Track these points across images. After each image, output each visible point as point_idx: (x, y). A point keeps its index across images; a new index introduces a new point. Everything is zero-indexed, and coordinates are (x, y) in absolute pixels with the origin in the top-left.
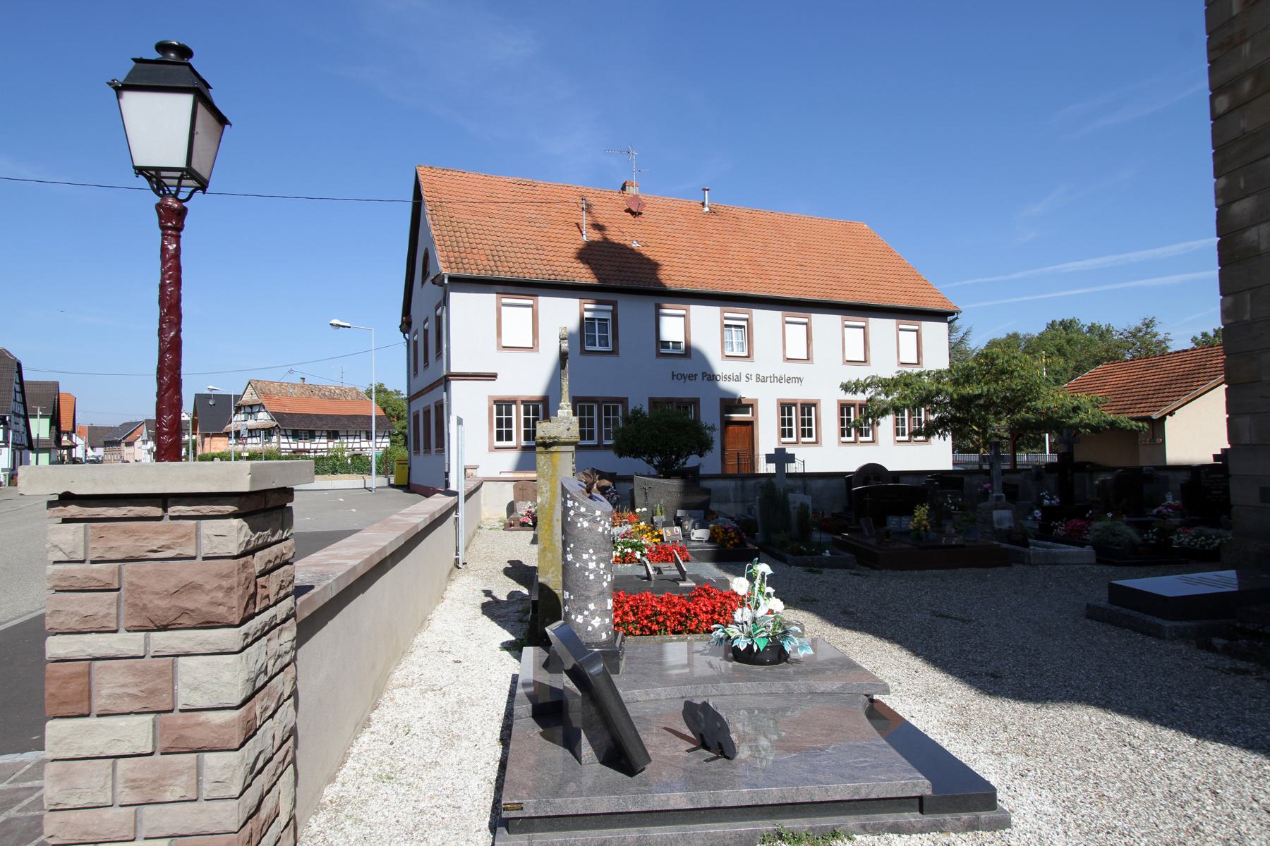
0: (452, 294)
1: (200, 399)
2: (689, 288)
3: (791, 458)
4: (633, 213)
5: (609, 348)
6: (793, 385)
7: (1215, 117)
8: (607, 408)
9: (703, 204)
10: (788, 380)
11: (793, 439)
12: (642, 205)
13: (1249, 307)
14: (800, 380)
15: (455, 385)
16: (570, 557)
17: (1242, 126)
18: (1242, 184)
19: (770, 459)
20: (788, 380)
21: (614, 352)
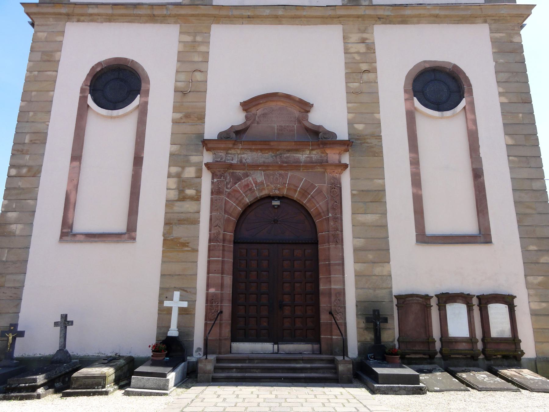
1: (36, 379)
7: (9, 176)
13: (6, 255)
16: (235, 370)
17: (19, 184)
18: (14, 206)
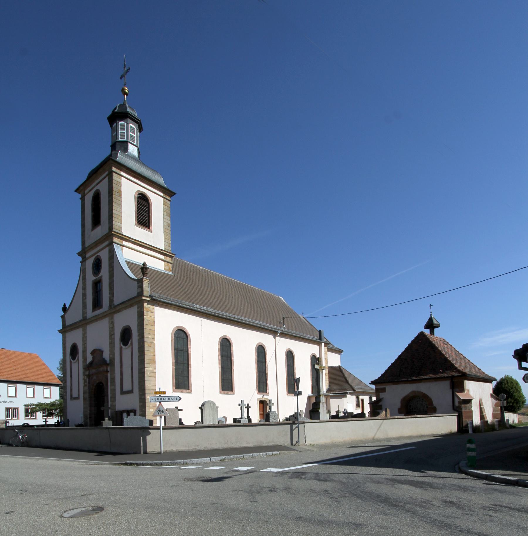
3: (8, 422)
10: (9, 402)
11: (10, 418)
14: (13, 402)
20: (9, 402)
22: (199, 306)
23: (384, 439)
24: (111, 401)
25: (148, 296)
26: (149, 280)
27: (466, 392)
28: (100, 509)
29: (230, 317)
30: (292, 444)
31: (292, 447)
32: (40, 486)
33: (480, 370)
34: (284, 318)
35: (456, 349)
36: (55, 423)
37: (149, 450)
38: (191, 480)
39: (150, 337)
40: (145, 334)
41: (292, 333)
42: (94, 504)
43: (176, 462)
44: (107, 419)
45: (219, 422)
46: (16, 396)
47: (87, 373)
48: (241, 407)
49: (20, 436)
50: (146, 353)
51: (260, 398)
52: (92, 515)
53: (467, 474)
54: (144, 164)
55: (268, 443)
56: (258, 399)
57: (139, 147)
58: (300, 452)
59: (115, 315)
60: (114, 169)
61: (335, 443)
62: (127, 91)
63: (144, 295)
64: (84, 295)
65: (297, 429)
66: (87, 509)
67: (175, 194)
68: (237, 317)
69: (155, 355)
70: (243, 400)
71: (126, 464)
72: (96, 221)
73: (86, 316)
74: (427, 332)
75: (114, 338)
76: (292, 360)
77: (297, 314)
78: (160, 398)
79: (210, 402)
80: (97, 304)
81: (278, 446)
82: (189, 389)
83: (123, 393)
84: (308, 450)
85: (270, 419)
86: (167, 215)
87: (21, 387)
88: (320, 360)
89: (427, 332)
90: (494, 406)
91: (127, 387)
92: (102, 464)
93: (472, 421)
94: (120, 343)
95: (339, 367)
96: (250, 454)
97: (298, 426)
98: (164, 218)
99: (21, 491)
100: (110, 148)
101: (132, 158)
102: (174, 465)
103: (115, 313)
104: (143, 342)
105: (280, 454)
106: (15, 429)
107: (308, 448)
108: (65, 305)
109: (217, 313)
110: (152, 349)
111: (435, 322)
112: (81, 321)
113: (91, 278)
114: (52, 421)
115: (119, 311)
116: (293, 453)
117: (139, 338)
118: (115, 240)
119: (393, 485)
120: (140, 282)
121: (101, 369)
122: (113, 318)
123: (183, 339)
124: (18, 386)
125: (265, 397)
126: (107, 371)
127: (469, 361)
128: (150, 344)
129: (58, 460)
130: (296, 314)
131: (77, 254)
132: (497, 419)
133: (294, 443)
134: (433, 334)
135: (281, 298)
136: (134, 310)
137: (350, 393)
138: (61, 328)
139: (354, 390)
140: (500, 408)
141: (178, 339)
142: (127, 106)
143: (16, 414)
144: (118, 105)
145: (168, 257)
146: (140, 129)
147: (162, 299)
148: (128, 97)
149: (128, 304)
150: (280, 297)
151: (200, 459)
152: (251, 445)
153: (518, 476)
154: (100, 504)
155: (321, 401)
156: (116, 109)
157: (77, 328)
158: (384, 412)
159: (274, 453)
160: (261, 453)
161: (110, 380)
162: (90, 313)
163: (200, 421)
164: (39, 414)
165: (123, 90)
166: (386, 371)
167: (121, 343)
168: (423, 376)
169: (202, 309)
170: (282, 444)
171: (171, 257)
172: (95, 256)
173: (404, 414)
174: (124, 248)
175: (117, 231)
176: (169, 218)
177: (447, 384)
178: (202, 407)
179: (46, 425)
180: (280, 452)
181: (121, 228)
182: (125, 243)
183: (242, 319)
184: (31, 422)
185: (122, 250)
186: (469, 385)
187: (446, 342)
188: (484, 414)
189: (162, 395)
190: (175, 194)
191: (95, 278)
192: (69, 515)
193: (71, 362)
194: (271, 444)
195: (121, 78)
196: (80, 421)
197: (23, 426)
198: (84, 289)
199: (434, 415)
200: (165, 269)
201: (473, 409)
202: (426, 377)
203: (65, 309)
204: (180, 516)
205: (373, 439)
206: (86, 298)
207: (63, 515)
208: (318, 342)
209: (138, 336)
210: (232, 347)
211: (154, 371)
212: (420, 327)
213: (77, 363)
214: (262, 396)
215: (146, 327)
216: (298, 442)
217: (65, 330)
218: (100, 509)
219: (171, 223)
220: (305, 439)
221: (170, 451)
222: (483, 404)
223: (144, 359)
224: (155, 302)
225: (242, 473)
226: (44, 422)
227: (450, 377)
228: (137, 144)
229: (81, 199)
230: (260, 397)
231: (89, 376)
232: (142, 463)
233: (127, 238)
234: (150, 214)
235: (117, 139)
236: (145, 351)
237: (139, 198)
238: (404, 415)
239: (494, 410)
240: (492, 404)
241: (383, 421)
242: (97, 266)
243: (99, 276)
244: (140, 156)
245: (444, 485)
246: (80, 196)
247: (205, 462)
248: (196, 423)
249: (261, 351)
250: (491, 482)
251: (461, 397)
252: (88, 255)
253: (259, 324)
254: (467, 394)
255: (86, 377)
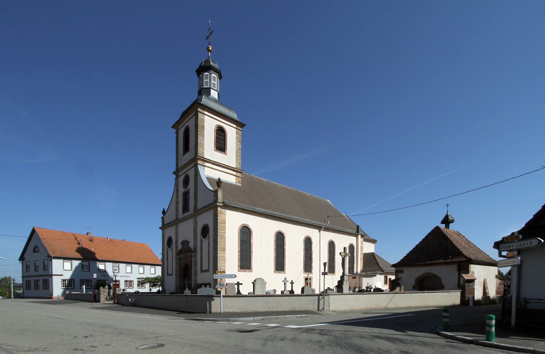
0: (161, 267)
2: (106, 260)
3: (126, 290)
4: (91, 241)
5: (88, 270)
6: (128, 277)
8: (87, 282)
9: (108, 238)
12: (93, 239)
15: (54, 277)
19: (122, 290)
21: (89, 271)
22: (260, 209)
23: (395, 308)
24: (194, 277)
25: (221, 202)
26: (222, 190)
27: (470, 273)
28: (162, 345)
29: (284, 216)
30: (318, 310)
31: (318, 312)
32: (132, 330)
33: (489, 256)
34: (328, 217)
35: (468, 239)
36: (157, 291)
37: (213, 310)
38: (232, 331)
39: (222, 232)
40: (218, 230)
41: (334, 228)
42: (160, 342)
43: (229, 319)
44: (187, 289)
45: (266, 293)
46: (131, 273)
47: (178, 257)
48: (285, 283)
49: (130, 300)
50: (219, 243)
51: (306, 276)
52: (156, 348)
53: (439, 334)
54: (222, 105)
55: (301, 309)
56: (304, 277)
57: (219, 91)
58: (323, 315)
59: (198, 217)
60: (199, 110)
61: (353, 310)
62: (210, 49)
63: (218, 202)
64: (177, 203)
65: (323, 299)
66: (154, 345)
67: (245, 125)
68: (290, 216)
69: (225, 245)
70: (286, 278)
71: (195, 320)
72: (186, 149)
73: (178, 218)
74: (443, 226)
75: (197, 233)
76: (333, 248)
77: (341, 212)
78: (221, 275)
79: (260, 279)
80: (186, 208)
81: (308, 311)
82: (250, 269)
83: (202, 271)
84: (330, 315)
85: (305, 291)
86: (239, 142)
87: (135, 266)
88: (345, 249)
89: (443, 226)
90: (498, 285)
91: (205, 267)
92: (179, 319)
93: (474, 297)
94: (201, 237)
95: (373, 254)
96: (283, 316)
97: (324, 297)
98: (236, 144)
99: (119, 333)
100: (197, 94)
101: (214, 100)
102: (227, 321)
103: (198, 214)
104: (217, 235)
105: (307, 316)
106: (126, 295)
107: (330, 313)
108: (164, 209)
109: (274, 214)
110: (223, 241)
111: (450, 218)
112: (174, 221)
113: (182, 190)
114: (155, 290)
115: (201, 213)
116: (317, 316)
117: (214, 233)
118: (199, 162)
119: (373, 339)
120: (216, 192)
121: (188, 255)
122: (196, 218)
123: (247, 233)
124: (133, 265)
125: (310, 275)
126: (192, 256)
127: (479, 249)
128: (222, 237)
129: (152, 316)
130: (339, 213)
131: (173, 173)
132: (500, 295)
133: (320, 309)
134: (448, 228)
135: (328, 201)
136: (211, 213)
137: (379, 273)
138: (161, 226)
139: (383, 271)
140: (503, 286)
141: (243, 233)
142: (211, 60)
143: (131, 284)
144: (204, 60)
145: (238, 173)
146: (220, 77)
147: (232, 204)
148: (211, 53)
149: (206, 208)
150: (327, 200)
151: (246, 318)
152: (287, 310)
153: (513, 339)
154: (163, 342)
155: (345, 279)
156: (202, 63)
157: (172, 225)
158: (398, 288)
159: (302, 315)
160: (292, 316)
161: (194, 263)
162: (181, 215)
163: (253, 292)
164: (147, 285)
165: (208, 48)
166: (405, 257)
167: (202, 236)
168: (435, 260)
169: (262, 211)
170: (311, 310)
171: (241, 173)
172: (185, 174)
173: (417, 290)
174: (206, 168)
175: (201, 156)
176: (240, 144)
177: (455, 267)
178: (254, 282)
179: (150, 293)
180: (307, 315)
181: (204, 153)
182: (206, 164)
183: (294, 218)
184: (141, 290)
185: (204, 169)
186: (474, 268)
187: (459, 234)
188: (487, 291)
189: (223, 274)
190: (245, 125)
191: (184, 190)
192: (142, 348)
193: (167, 249)
194: (302, 309)
195: (207, 39)
196: (173, 290)
197: (135, 292)
198: (177, 198)
199: (442, 291)
200: (236, 182)
201: (476, 287)
202: (437, 262)
203: (164, 212)
204: (210, 352)
205: (385, 308)
206: (178, 204)
207: (138, 348)
208: (356, 235)
209: (214, 231)
210: (285, 239)
211: (225, 256)
212: (437, 222)
213: (172, 250)
214: (307, 275)
215: (219, 225)
216: (323, 309)
217: (164, 227)
218: (162, 345)
219: (241, 147)
220: (329, 306)
221: (227, 312)
222: (487, 283)
223: (217, 248)
224: (226, 206)
225: (270, 328)
226: (523, 298)
227: (458, 262)
228: (218, 90)
229: (176, 133)
230: (306, 275)
231: (179, 259)
232: (206, 319)
233: (208, 160)
234: (226, 142)
235: (202, 86)
236: (218, 242)
237: (217, 130)
238: (418, 291)
239: (498, 288)
240: (497, 283)
241: (394, 295)
242: (186, 181)
243: (188, 188)
244: (220, 98)
245: (412, 341)
246: (175, 130)
247: (250, 320)
248: (249, 293)
249: (308, 242)
250: (453, 341)
251: (465, 278)
252: (180, 174)
253: (307, 222)
254: (471, 275)
255: (177, 260)
